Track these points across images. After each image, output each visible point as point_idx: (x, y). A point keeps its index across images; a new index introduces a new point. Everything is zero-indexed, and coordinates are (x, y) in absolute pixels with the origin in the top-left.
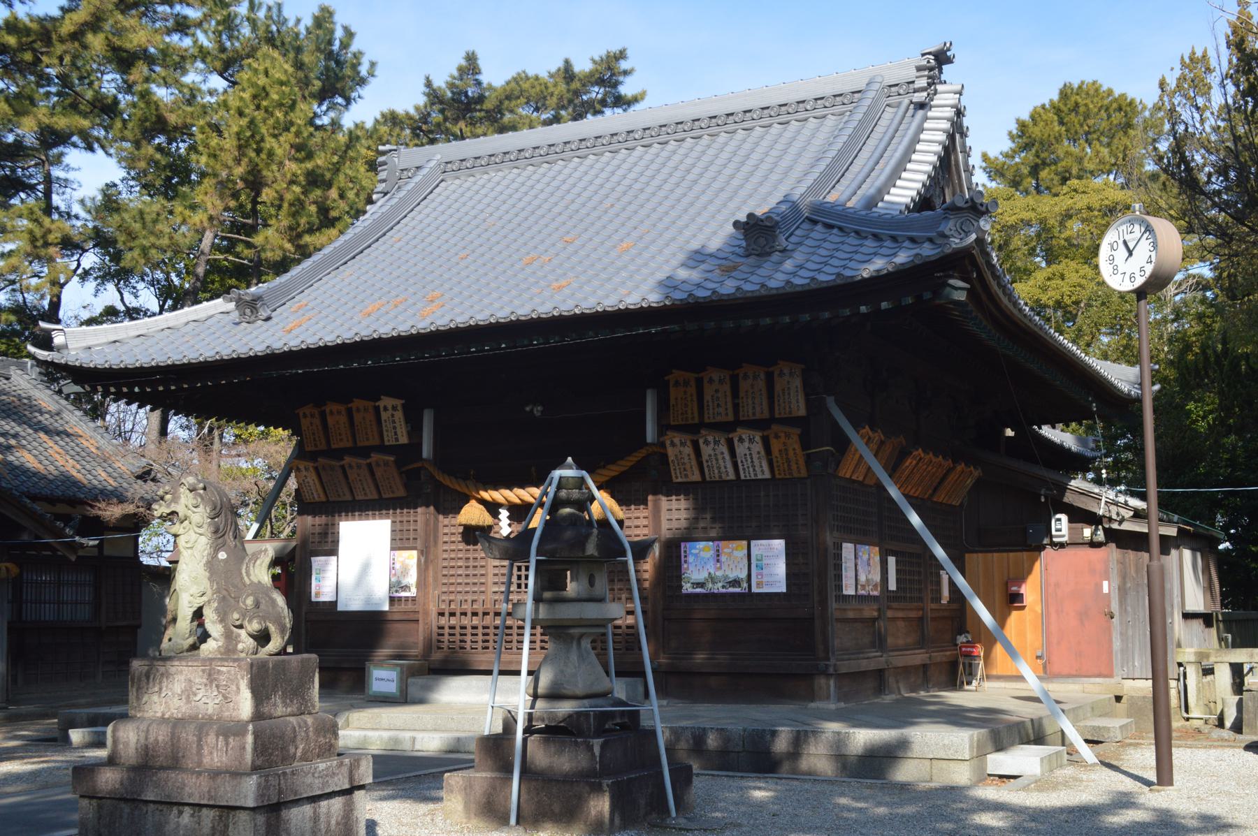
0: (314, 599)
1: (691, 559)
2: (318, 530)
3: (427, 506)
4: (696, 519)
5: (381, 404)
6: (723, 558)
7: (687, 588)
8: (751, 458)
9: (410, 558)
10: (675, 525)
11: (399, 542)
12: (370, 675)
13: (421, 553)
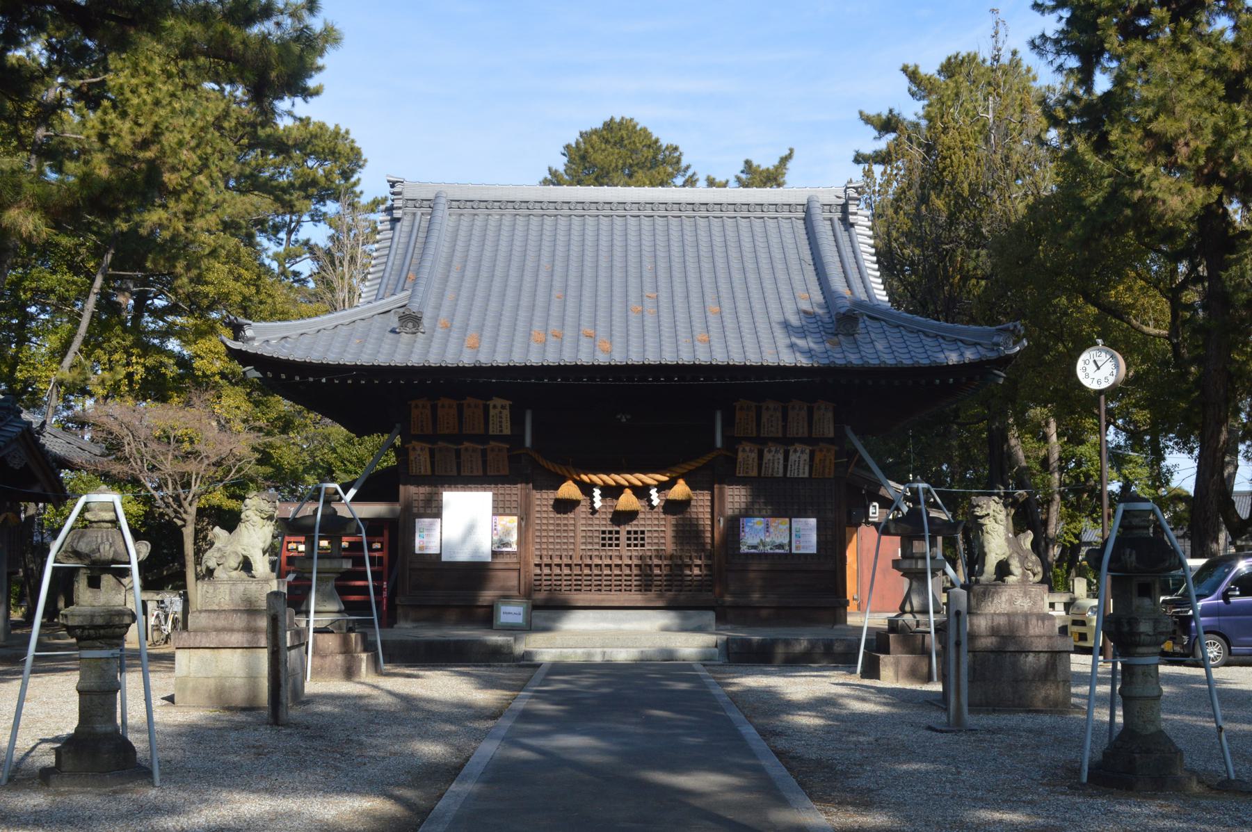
0: (417, 551)
1: (747, 529)
2: (422, 497)
3: (527, 483)
4: (752, 503)
5: (491, 403)
6: (771, 530)
7: (744, 549)
8: (800, 463)
9: (511, 522)
10: (737, 506)
11: (499, 509)
12: (498, 610)
13: (521, 519)
